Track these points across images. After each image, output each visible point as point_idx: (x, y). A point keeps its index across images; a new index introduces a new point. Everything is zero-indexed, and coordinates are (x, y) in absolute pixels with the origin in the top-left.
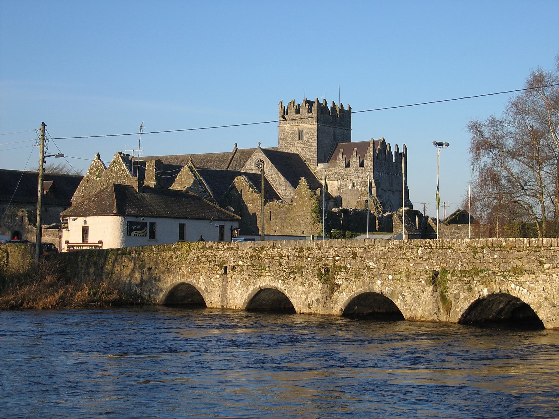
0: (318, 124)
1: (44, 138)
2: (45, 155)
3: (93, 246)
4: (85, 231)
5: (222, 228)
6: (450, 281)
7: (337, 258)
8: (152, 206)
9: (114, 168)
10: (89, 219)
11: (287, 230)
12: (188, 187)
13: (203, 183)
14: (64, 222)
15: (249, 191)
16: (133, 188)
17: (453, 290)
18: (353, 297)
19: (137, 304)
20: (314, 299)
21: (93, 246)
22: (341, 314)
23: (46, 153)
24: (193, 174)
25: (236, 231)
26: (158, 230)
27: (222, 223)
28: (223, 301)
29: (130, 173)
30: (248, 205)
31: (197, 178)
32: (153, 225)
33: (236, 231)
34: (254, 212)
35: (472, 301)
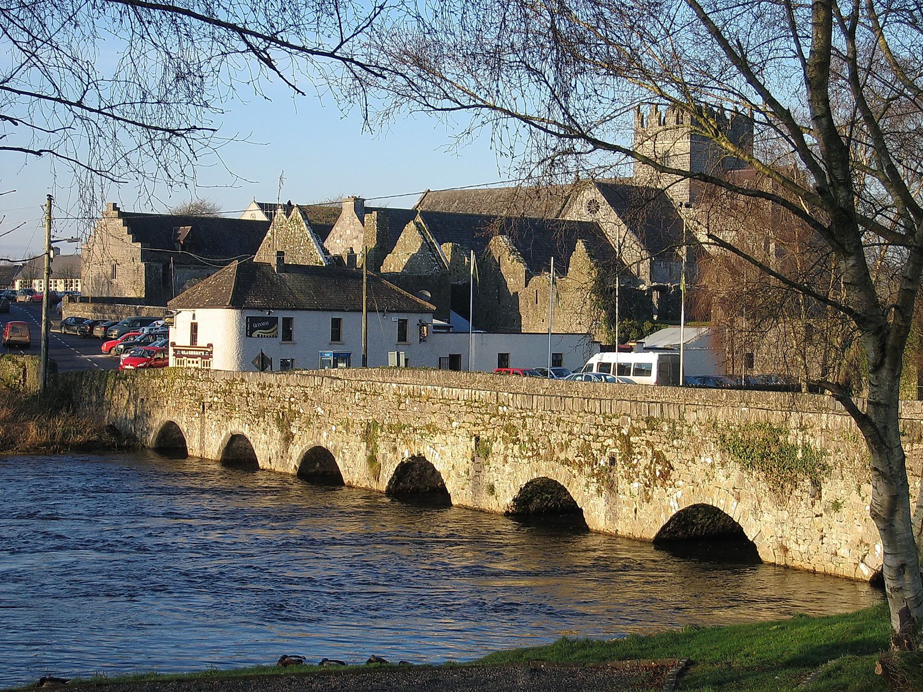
0: (691, 142)
1: (50, 217)
2: (52, 239)
3: (202, 351)
4: (194, 328)
5: (403, 325)
6: (380, 437)
7: (292, 400)
8: (291, 293)
9: (291, 229)
10: (199, 312)
11: (559, 319)
12: (413, 254)
13: (435, 247)
14: (169, 316)
15: (509, 260)
16: (271, 266)
17: (383, 449)
18: (305, 452)
19: (120, 448)
20: (274, 452)
21: (202, 351)
22: (296, 473)
23: (53, 237)
24: (422, 234)
25: (425, 328)
26: (296, 327)
27: (403, 316)
28: (201, 448)
29: (312, 237)
30: (508, 280)
31: (426, 241)
32: (288, 322)
33: (425, 328)
34: (514, 291)
35: (396, 465)
